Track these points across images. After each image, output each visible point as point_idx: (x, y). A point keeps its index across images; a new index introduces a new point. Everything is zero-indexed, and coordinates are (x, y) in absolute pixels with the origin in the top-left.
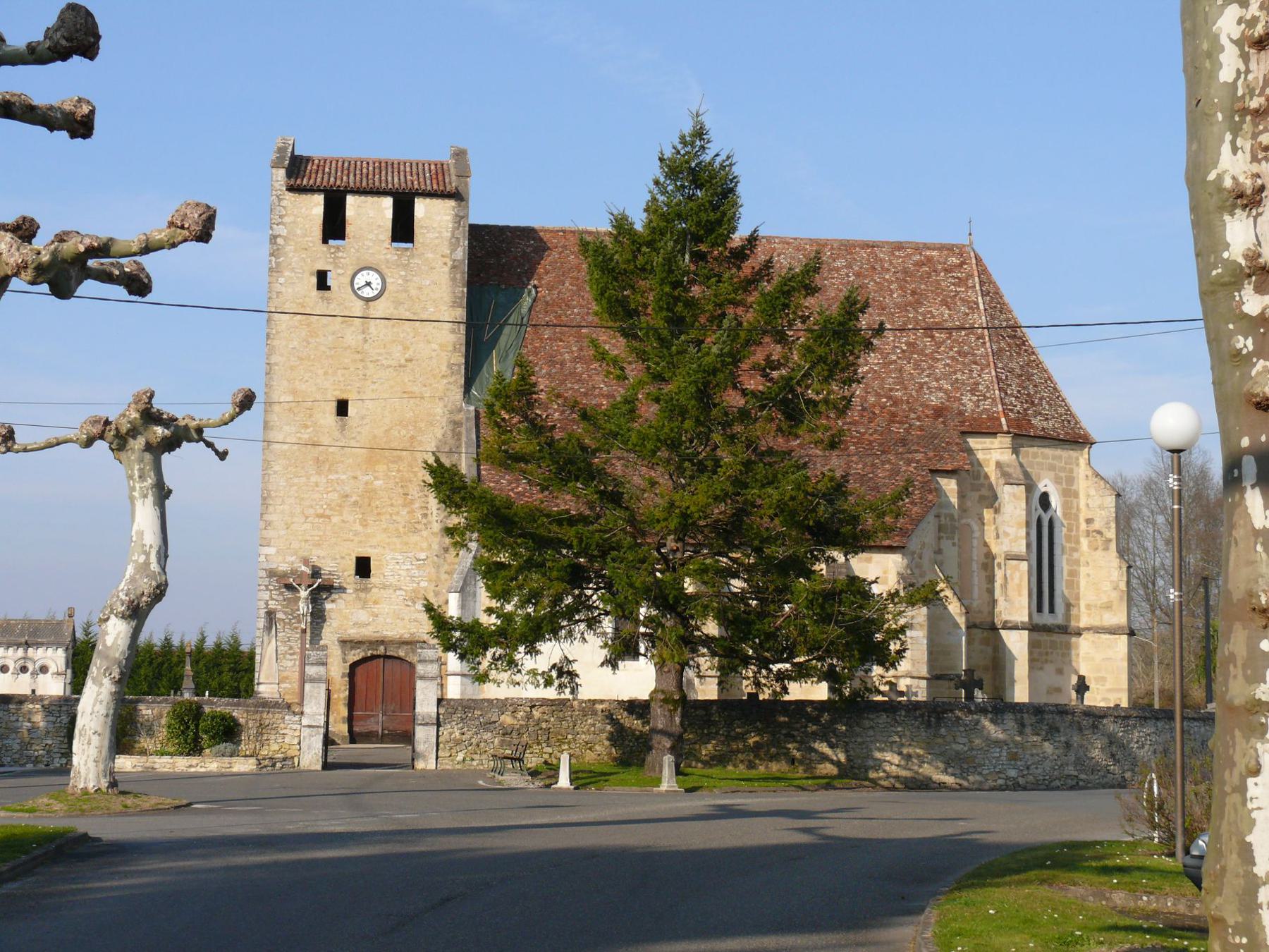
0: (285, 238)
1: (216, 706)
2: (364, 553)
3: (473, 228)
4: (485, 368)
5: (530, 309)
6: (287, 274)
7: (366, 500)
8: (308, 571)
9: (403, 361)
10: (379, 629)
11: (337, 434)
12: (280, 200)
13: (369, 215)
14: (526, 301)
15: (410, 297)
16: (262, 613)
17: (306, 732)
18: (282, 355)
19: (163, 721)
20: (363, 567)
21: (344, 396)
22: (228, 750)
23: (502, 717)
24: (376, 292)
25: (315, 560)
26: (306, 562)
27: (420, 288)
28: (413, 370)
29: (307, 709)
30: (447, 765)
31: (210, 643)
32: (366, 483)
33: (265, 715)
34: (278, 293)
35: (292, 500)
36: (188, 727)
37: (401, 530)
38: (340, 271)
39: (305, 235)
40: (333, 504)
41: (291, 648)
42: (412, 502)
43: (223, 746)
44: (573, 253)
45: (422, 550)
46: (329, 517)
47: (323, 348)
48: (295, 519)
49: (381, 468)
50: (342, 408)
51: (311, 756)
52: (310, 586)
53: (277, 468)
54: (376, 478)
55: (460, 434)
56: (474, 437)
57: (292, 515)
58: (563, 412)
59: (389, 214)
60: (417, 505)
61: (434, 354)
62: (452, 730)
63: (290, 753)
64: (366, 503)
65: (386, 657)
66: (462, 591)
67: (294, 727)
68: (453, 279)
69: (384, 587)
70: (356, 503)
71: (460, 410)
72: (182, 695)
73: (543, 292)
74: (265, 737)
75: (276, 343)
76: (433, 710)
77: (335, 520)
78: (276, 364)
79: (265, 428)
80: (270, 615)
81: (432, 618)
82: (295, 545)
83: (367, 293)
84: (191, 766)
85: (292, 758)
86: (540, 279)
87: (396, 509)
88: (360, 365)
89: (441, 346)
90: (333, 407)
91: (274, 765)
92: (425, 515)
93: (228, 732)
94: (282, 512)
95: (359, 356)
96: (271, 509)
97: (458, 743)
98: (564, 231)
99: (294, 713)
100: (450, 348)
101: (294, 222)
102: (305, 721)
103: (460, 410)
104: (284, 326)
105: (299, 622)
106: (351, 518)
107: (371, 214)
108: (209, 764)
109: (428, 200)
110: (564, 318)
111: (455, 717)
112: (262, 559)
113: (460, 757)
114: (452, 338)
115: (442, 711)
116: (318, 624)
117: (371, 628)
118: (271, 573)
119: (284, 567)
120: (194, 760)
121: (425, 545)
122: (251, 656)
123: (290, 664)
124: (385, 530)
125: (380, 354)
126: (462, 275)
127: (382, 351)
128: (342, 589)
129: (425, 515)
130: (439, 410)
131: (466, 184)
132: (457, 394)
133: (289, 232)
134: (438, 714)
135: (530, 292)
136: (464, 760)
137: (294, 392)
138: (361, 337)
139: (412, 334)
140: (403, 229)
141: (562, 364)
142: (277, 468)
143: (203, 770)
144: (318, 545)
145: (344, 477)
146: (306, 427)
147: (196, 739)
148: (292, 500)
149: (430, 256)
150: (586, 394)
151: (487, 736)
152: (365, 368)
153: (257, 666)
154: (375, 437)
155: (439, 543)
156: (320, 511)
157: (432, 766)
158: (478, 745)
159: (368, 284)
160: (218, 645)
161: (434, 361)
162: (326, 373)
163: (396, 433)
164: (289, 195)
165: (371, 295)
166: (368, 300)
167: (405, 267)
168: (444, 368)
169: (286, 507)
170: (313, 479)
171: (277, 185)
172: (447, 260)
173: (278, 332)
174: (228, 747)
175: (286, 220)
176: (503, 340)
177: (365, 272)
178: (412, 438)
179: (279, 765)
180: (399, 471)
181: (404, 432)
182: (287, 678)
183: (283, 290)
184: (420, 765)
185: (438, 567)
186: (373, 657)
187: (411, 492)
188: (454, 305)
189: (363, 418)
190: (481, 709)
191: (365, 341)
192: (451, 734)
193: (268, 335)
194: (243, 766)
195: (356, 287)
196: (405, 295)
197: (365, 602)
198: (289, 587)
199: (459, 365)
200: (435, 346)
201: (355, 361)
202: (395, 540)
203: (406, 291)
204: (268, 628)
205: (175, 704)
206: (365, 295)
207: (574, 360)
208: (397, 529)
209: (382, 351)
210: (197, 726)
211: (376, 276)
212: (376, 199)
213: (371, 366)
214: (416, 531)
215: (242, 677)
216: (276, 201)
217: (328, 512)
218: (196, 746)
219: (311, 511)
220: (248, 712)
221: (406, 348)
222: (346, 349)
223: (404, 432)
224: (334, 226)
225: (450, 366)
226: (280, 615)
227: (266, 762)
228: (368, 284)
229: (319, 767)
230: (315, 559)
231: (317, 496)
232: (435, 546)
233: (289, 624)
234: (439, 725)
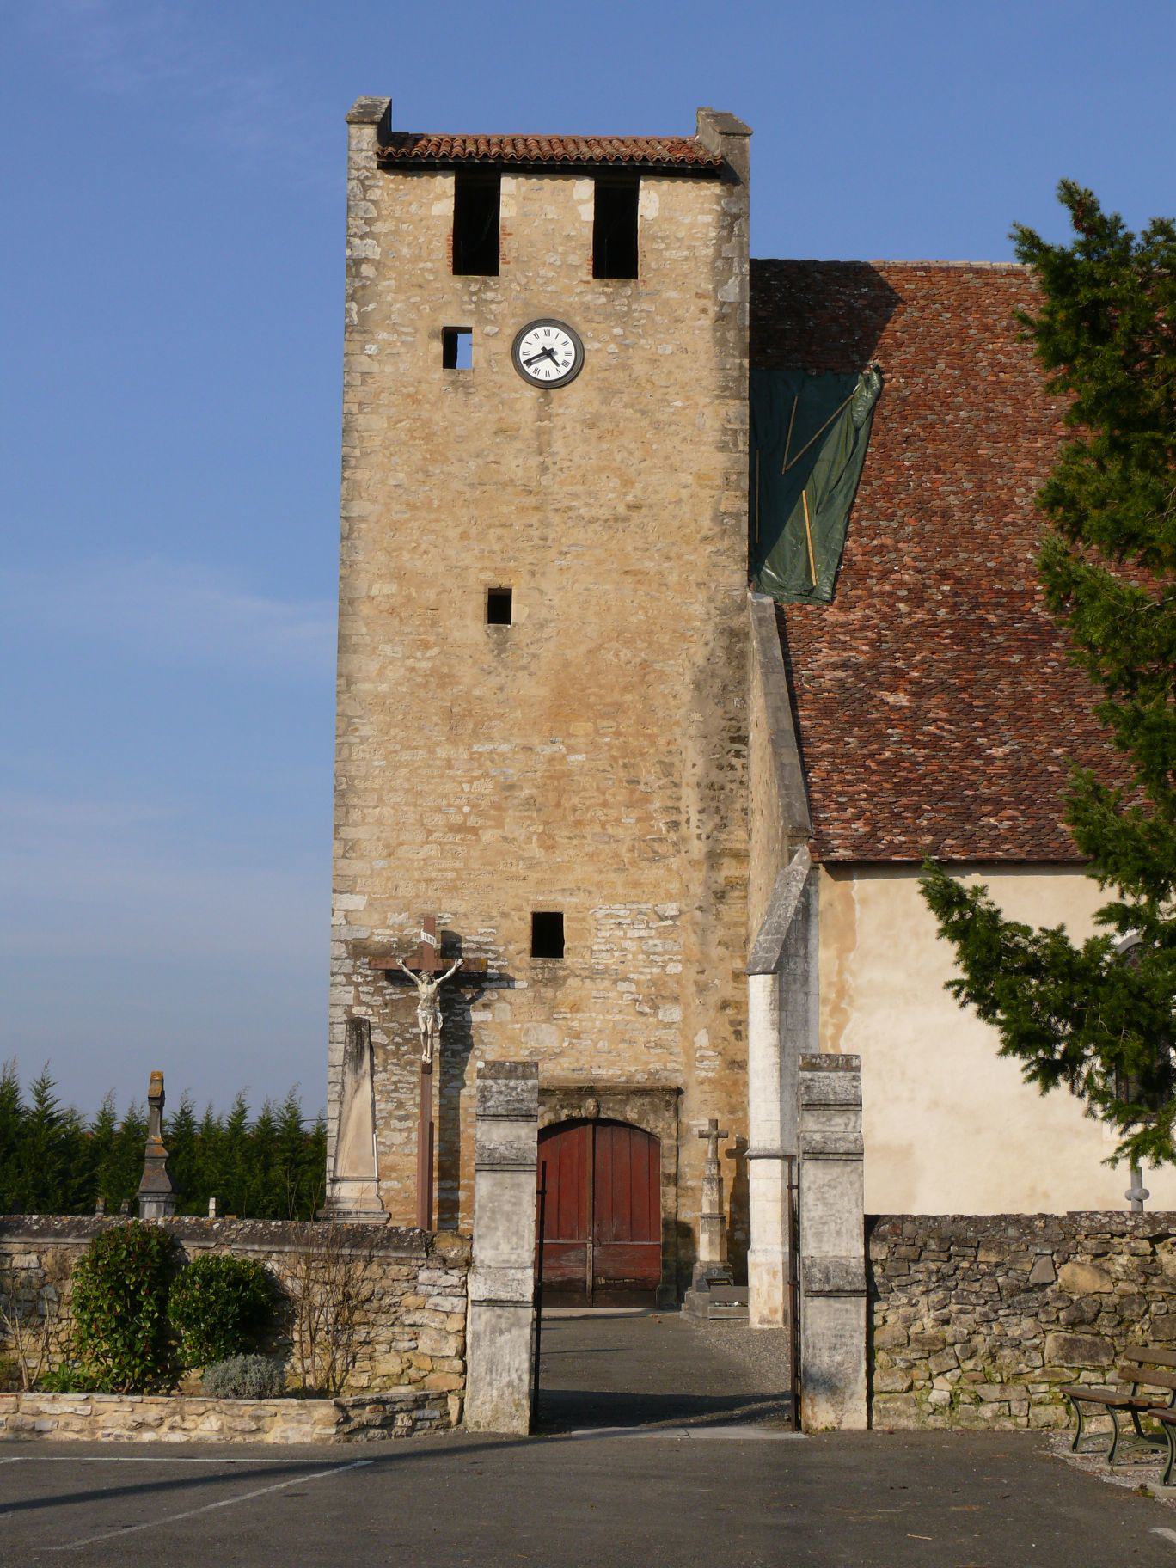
0: (378, 265)
1: (221, 1241)
2: (549, 902)
3: (754, 264)
4: (787, 529)
5: (871, 412)
6: (382, 335)
7: (552, 796)
8: (433, 942)
9: (621, 510)
10: (584, 1061)
11: (488, 659)
12: (366, 189)
13: (548, 219)
14: (863, 396)
15: (635, 381)
16: (341, 1031)
17: (480, 1319)
18: (374, 501)
19: (69, 1288)
20: (548, 934)
21: (502, 582)
22: (253, 1376)
23: (1065, 1271)
24: (564, 370)
25: (447, 920)
26: (429, 923)
27: (653, 361)
28: (643, 527)
29: (483, 1252)
30: (902, 1417)
31: (252, 1119)
32: (551, 760)
33: (358, 1270)
34: (365, 375)
35: (398, 798)
36: (136, 1307)
37: (626, 856)
38: (489, 329)
39: (416, 259)
40: (484, 804)
41: (400, 1105)
42: (646, 798)
43: (235, 1364)
44: (947, 309)
45: (670, 897)
46: (474, 831)
47: (456, 485)
48: (405, 837)
49: (582, 728)
50: (499, 607)
51: (496, 1396)
52: (438, 974)
53: (366, 731)
54: (572, 749)
55: (742, 655)
56: (778, 653)
57: (400, 827)
58: (954, 608)
59: (588, 212)
60: (657, 805)
61: (684, 493)
62: (913, 1311)
63: (436, 1383)
64: (552, 801)
65: (598, 1122)
66: (779, 970)
67: (447, 1304)
68: (721, 343)
69: (593, 975)
70: (529, 802)
71: (742, 607)
72: (135, 1210)
73: (895, 380)
74: (360, 1336)
75: (362, 475)
76: (852, 1248)
77: (488, 836)
78: (362, 519)
79: (340, 649)
80: (358, 1027)
81: (954, 931)
82: (407, 890)
83: (546, 370)
84: (141, 1426)
85: (443, 1397)
86: (886, 357)
87: (613, 813)
88: (534, 519)
89: (699, 477)
90: (479, 603)
91: (387, 1423)
92: (674, 825)
93: (251, 1322)
94: (379, 821)
95: (532, 501)
96: (355, 815)
97: (932, 1347)
98: (927, 270)
99: (446, 1264)
100: (718, 482)
101: (396, 232)
102: (478, 1288)
103: (742, 607)
104: (377, 441)
105: (417, 1050)
106: (520, 834)
107: (552, 212)
108: (197, 1421)
109: (666, 185)
110: (939, 428)
111: (919, 1271)
112: (339, 919)
113: (940, 1392)
114: (720, 460)
115: (879, 1252)
116: (455, 1054)
117: (566, 1062)
118: (358, 949)
119: (383, 936)
120: (151, 1407)
121: (674, 887)
122: (320, 1139)
123: (398, 1138)
124: (591, 857)
125: (575, 496)
126: (739, 336)
127: (579, 488)
128: (505, 981)
129: (674, 825)
130: (698, 609)
131: (743, 150)
132: (735, 575)
133: (385, 253)
134: (869, 1263)
135: (868, 381)
136: (953, 1401)
137: (399, 575)
138: (534, 461)
139: (638, 454)
140: (616, 251)
141: (946, 513)
142: (366, 731)
143: (177, 1437)
144: (453, 889)
145: (504, 748)
146: (426, 646)
147: (162, 1340)
148: (398, 798)
149: (673, 295)
150: (998, 572)
151: (1021, 1327)
152: (545, 523)
153: (331, 1151)
154: (566, 664)
155: (705, 883)
156: (459, 819)
157: (855, 1419)
158: (993, 1356)
159: (548, 354)
160: (266, 1122)
161: (686, 508)
162: (464, 536)
163: (610, 656)
164: (385, 179)
165: (554, 376)
166: (547, 386)
167: (623, 318)
168: (706, 522)
169: (387, 811)
170: (441, 753)
171: (360, 159)
172: (708, 303)
173: (365, 454)
174: (254, 1366)
175: (379, 227)
176: (820, 471)
177: (540, 330)
178: (644, 665)
179: (402, 1421)
180: (618, 734)
181: (626, 654)
182: (392, 1168)
183: (375, 368)
184: (820, 1414)
185: (703, 932)
186: (572, 1123)
187: (644, 776)
188: (724, 393)
189: (542, 626)
190: (999, 1247)
191: (544, 469)
192: (909, 1321)
193: (345, 460)
194: (297, 1427)
195: (523, 358)
196: (622, 375)
197: (554, 1008)
198: (396, 977)
199: (737, 516)
200: (687, 478)
201: (522, 510)
202: (612, 876)
203: (625, 367)
204: (355, 1057)
205: (101, 1238)
206: (541, 376)
207: (968, 507)
208: (617, 855)
209: (579, 488)
210: (162, 1302)
211: (564, 336)
212: (559, 183)
213: (556, 519)
214: (656, 858)
215: (304, 1173)
216: (358, 191)
217: (472, 821)
218: (159, 1360)
219: (438, 819)
220: (309, 1259)
221: (628, 483)
222: (504, 485)
223: (626, 654)
224: (476, 246)
225: (718, 517)
226: (377, 1037)
227: (366, 1415)
228: (548, 354)
229: (519, 1425)
230: (447, 918)
231: (450, 787)
232: (697, 890)
233: (396, 1054)
234: (872, 1295)
